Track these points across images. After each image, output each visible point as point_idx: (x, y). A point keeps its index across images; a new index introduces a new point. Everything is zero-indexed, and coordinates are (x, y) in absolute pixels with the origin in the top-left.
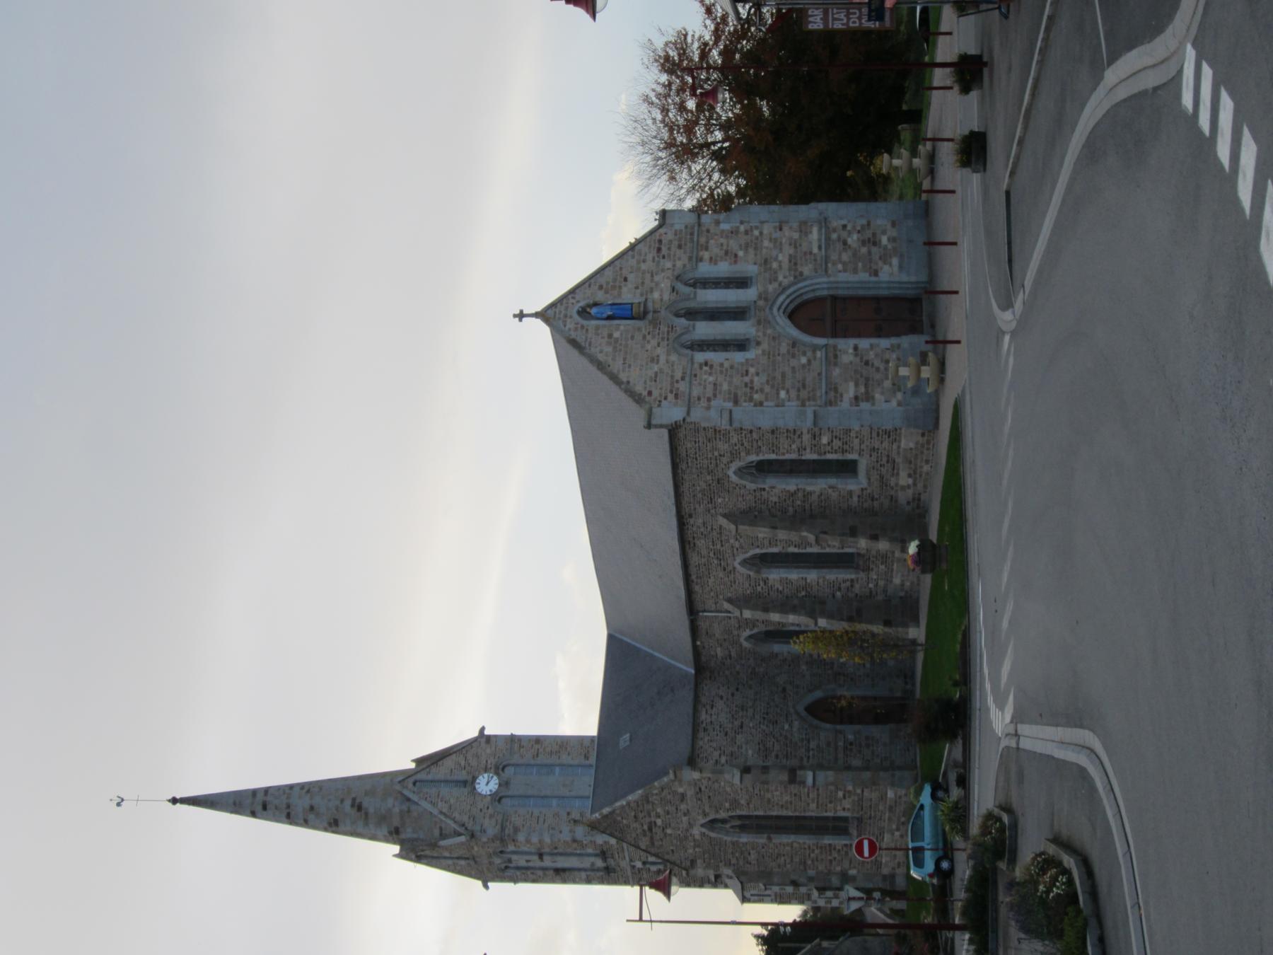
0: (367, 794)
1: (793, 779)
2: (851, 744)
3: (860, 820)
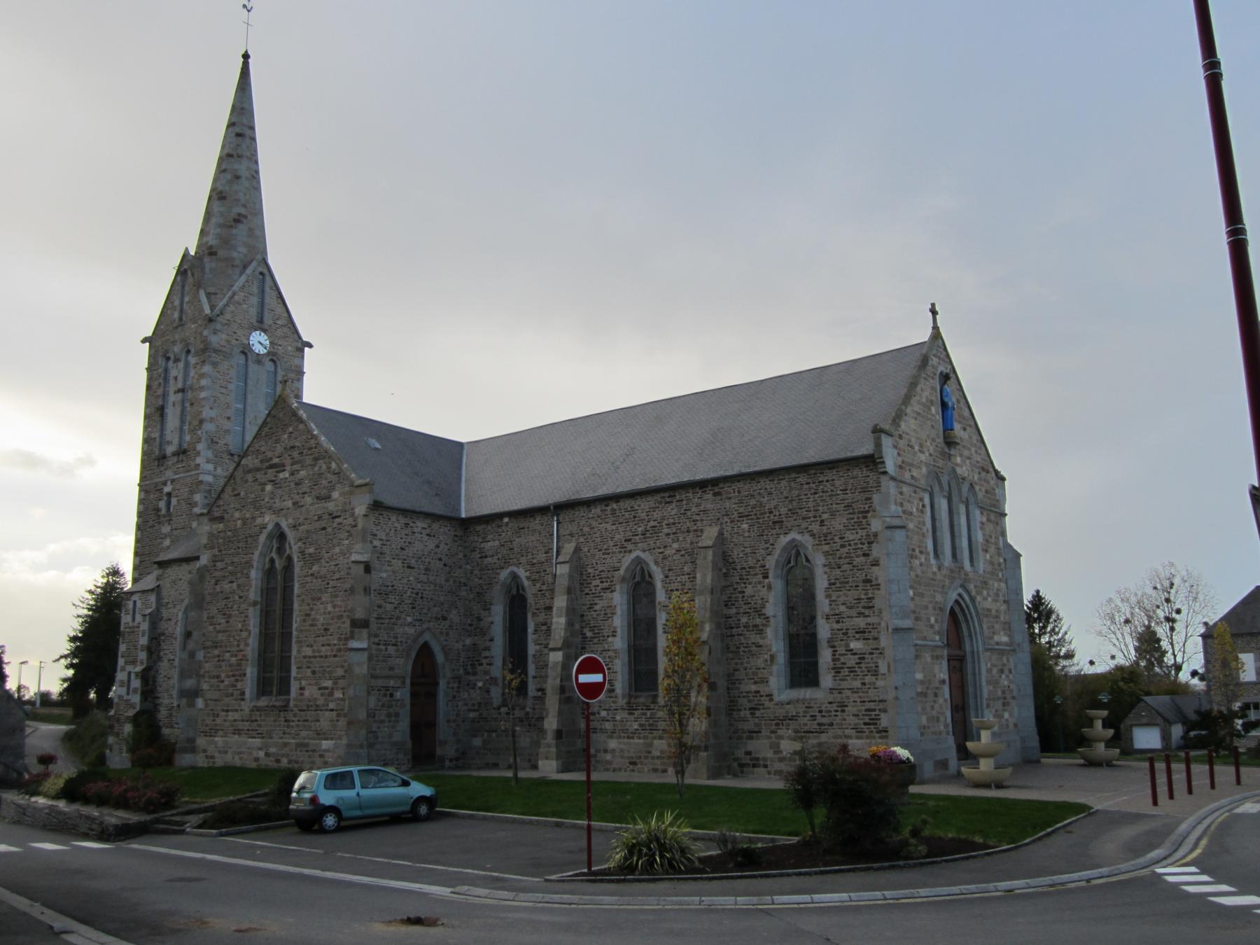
0: (250, 229)
1: (359, 624)
2: (391, 695)
3: (285, 708)
